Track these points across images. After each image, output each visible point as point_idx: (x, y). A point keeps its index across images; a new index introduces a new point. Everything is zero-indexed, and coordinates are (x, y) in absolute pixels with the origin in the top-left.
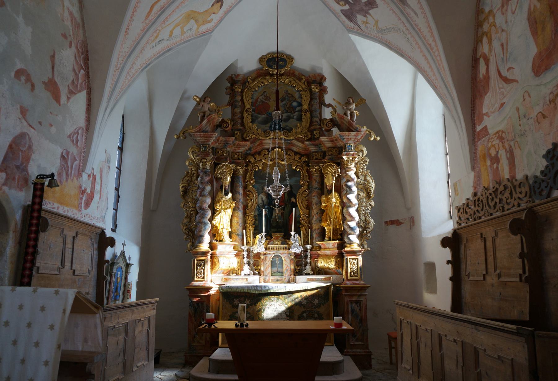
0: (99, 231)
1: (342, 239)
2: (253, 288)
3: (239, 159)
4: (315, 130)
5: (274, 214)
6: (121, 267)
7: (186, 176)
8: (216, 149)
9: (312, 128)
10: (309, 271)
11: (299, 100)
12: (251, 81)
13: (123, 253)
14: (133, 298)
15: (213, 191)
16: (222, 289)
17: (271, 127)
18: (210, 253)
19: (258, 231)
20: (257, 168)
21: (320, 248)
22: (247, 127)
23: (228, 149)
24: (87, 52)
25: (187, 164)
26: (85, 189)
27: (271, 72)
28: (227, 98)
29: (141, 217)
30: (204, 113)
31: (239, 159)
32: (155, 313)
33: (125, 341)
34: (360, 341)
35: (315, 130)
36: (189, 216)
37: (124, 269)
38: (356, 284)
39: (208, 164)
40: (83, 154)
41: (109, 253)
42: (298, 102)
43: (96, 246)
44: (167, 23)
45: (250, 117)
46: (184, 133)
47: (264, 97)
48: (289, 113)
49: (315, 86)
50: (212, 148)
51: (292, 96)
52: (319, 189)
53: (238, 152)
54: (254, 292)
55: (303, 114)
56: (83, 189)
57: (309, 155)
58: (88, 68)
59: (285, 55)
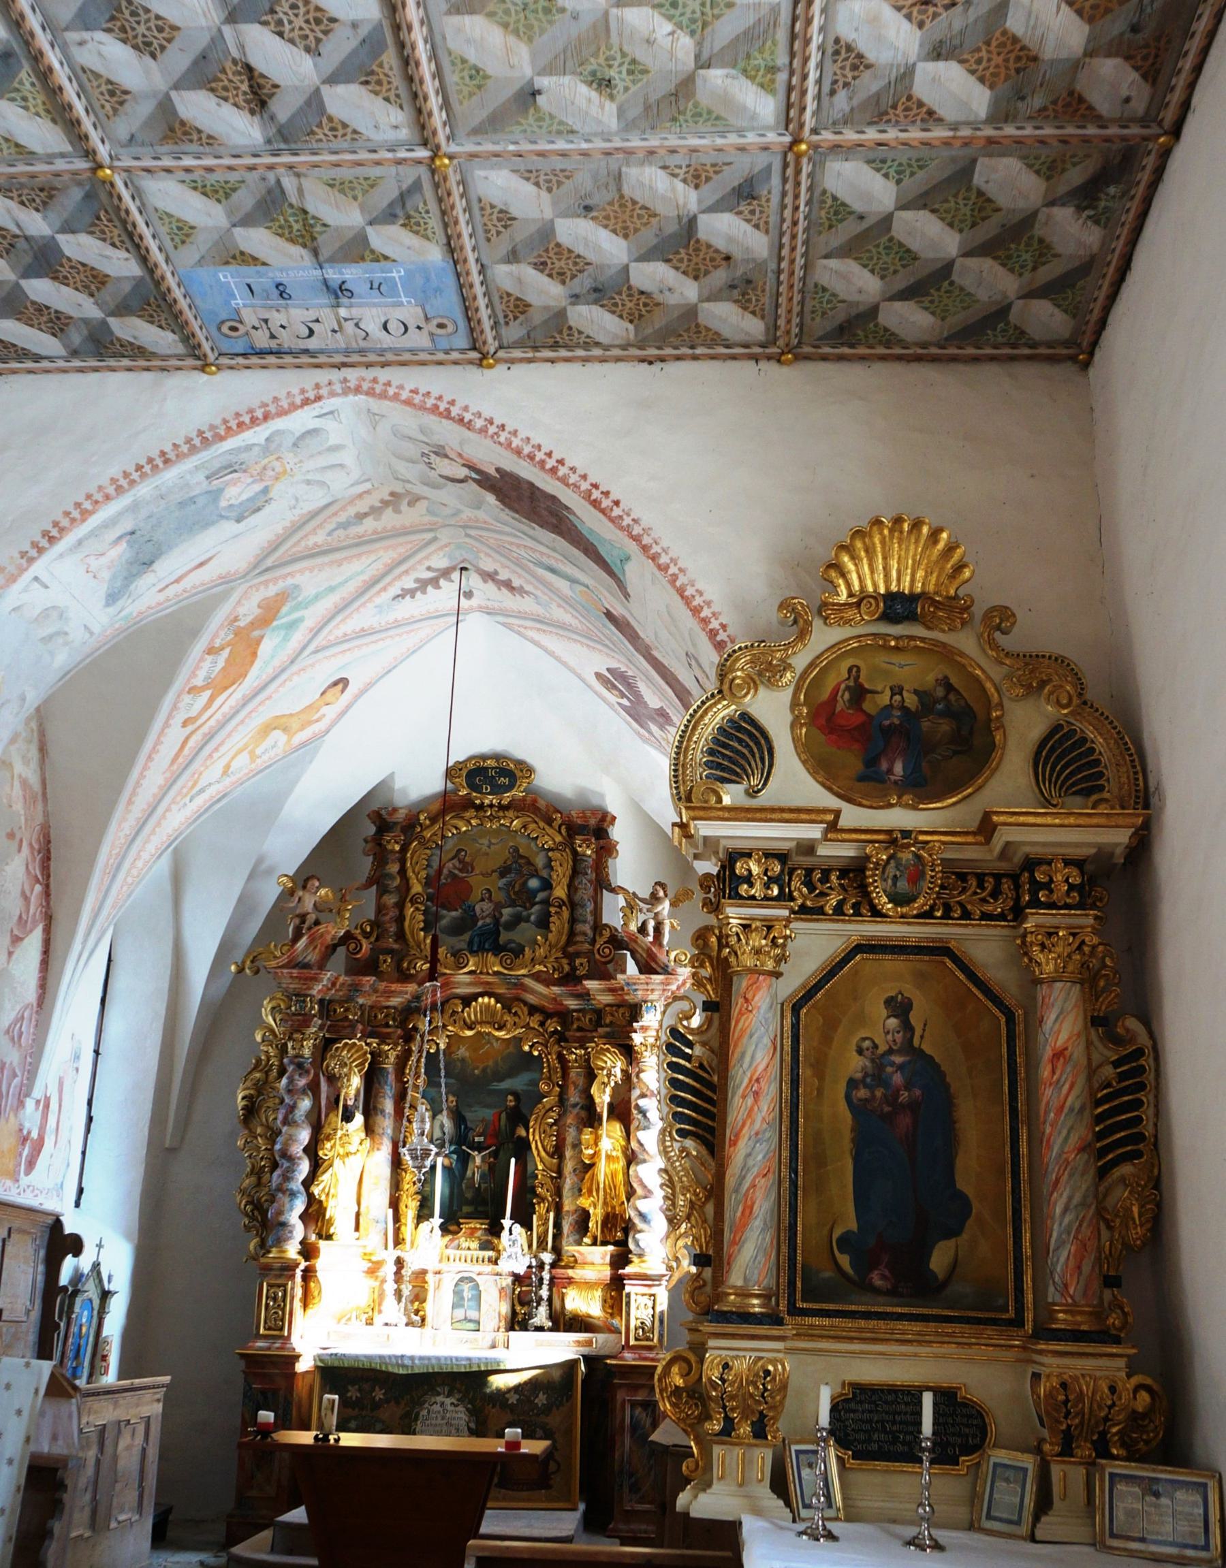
0: (50, 1220)
1: (622, 1244)
2: (394, 1361)
3: (387, 1025)
4: (578, 954)
5: (471, 1166)
6: (91, 1301)
7: (254, 1069)
8: (330, 1001)
9: (571, 949)
10: (544, 1320)
11: (544, 874)
12: (428, 822)
13: (96, 1266)
14: (110, 1378)
15: (316, 1116)
16: (321, 1360)
17: (470, 943)
18: (302, 1267)
19: (424, 1214)
20: (434, 1047)
21: (575, 1263)
22: (412, 943)
23: (361, 1001)
24: (49, 842)
25: (259, 1038)
26: (29, 1133)
27: (478, 802)
28: (366, 864)
29: (141, 1169)
30: (303, 917)
31: (387, 1025)
32: (160, 1410)
33: (98, 1462)
34: (649, 1503)
35: (578, 954)
36: (256, 1170)
37: (96, 1303)
38: (646, 1359)
39: (308, 1044)
40: (29, 1060)
41: (69, 1265)
42: (542, 879)
43: (42, 1253)
44: (216, 755)
45: (422, 917)
46: (255, 960)
47: (457, 864)
48: (519, 909)
49: (584, 841)
50: (321, 1002)
51: (529, 863)
52: (582, 1108)
53: (387, 1007)
54: (396, 1371)
55: (553, 910)
56: (25, 1132)
57: (564, 1016)
58: (49, 876)
59: (510, 759)
